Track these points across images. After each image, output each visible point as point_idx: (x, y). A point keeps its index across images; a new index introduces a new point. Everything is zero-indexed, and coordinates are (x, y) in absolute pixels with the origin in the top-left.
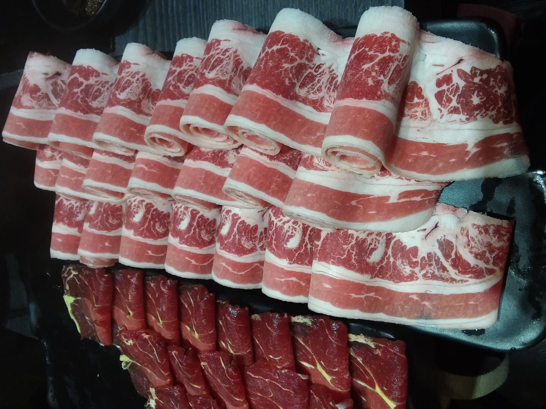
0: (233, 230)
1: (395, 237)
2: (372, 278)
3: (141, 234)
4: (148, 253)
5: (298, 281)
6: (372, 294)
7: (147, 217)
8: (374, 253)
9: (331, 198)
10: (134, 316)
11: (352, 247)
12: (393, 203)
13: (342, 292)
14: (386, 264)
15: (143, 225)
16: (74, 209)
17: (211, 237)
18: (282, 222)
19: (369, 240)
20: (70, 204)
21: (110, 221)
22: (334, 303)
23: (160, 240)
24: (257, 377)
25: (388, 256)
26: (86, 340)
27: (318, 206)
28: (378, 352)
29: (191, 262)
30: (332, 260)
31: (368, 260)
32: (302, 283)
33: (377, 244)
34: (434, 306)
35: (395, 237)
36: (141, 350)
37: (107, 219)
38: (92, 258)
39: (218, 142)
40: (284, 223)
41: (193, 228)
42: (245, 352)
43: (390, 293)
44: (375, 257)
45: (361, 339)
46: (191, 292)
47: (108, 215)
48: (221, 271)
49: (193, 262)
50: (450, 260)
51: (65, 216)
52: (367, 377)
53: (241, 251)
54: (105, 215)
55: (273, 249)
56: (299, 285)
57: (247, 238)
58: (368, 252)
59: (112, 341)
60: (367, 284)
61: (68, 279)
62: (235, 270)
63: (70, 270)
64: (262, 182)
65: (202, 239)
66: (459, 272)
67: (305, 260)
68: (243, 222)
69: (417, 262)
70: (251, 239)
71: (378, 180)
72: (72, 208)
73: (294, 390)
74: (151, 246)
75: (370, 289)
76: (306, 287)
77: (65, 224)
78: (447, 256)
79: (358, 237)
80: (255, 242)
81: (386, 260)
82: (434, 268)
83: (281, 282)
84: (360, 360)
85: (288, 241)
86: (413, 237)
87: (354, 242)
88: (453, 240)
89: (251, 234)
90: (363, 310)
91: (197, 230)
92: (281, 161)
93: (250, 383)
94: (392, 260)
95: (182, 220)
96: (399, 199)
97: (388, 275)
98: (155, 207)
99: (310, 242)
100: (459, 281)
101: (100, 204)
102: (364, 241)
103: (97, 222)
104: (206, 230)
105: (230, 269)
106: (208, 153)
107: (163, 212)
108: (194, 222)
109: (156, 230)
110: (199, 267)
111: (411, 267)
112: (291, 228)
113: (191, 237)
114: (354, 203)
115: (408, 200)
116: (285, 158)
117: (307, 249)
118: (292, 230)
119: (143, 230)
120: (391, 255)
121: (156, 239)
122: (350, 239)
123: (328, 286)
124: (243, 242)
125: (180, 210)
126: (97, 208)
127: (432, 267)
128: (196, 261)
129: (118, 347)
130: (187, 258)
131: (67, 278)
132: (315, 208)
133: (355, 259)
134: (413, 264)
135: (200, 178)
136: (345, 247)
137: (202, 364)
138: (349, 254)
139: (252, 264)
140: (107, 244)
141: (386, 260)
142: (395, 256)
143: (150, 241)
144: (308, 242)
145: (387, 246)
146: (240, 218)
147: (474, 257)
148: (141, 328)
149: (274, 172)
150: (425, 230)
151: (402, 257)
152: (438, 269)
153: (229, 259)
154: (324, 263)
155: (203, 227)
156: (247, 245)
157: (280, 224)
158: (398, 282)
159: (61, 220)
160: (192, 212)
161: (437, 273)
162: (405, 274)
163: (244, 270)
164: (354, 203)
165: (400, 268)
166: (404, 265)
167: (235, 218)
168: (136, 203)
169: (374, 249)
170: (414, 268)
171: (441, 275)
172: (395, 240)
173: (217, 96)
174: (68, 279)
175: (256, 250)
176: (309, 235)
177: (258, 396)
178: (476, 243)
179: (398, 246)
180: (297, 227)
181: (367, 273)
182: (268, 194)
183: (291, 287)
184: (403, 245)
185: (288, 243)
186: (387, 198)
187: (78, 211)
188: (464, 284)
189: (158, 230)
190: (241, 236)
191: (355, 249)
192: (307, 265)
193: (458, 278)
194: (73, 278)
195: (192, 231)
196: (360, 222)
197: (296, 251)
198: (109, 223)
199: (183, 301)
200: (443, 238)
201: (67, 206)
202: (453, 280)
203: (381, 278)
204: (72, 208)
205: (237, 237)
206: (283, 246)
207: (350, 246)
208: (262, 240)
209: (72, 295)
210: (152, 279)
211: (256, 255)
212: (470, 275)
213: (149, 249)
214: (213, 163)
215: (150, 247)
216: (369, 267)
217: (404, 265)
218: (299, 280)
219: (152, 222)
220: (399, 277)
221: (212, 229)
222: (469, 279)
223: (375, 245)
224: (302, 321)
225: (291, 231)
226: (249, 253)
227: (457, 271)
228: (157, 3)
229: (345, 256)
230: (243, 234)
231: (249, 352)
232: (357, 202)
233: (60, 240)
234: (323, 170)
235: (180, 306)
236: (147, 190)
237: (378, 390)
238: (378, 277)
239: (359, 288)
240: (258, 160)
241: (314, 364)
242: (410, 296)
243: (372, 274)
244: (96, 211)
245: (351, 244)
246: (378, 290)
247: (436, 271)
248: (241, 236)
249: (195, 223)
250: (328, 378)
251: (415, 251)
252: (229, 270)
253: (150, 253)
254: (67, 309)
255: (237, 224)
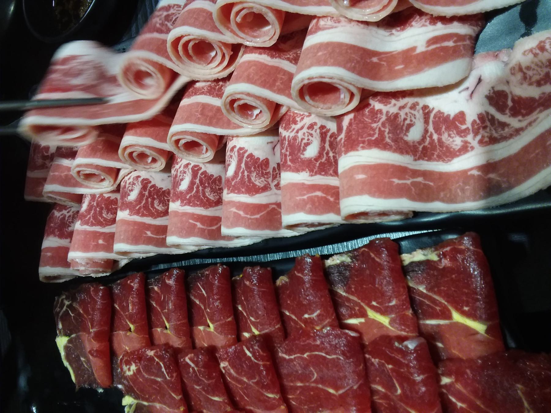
0: (241, 167)
1: (433, 109)
2: (415, 160)
3: (138, 213)
4: (146, 234)
5: (324, 195)
6: (420, 179)
7: (144, 194)
8: (412, 130)
9: (347, 52)
10: (136, 331)
11: (383, 124)
12: (422, 53)
13: (380, 180)
14: (430, 143)
15: (140, 203)
16: (66, 219)
17: (218, 197)
18: (295, 131)
19: (402, 114)
20: (61, 215)
21: (104, 215)
22: (372, 194)
23: (160, 219)
24: (292, 357)
25: (429, 134)
26: (82, 389)
27: (332, 61)
28: (446, 262)
29: (197, 225)
30: (361, 145)
31: (406, 138)
32: (329, 197)
33: (413, 119)
34: (501, 175)
35: (433, 109)
36: (146, 376)
37: (101, 213)
38: (82, 258)
39: (212, 69)
40: (297, 132)
41: (195, 186)
42: (273, 328)
43: (442, 175)
44: (414, 135)
45: (419, 256)
46: (202, 281)
47: (102, 209)
48: (231, 219)
49: (199, 225)
50: (507, 111)
51: (56, 228)
52: (438, 308)
53: (253, 190)
54: (98, 209)
55: (290, 166)
56: (327, 201)
57: (257, 174)
58: (404, 128)
59: (112, 381)
60: (411, 167)
61: (61, 314)
62: (247, 214)
63: (62, 300)
64: (265, 80)
65: (207, 197)
66: (524, 116)
67: (329, 170)
68: (251, 156)
69: (468, 129)
70: (263, 175)
71: (397, 36)
72: (64, 218)
73: (343, 353)
74: (150, 226)
75: (415, 173)
76: (335, 202)
77: (55, 236)
78: (501, 109)
79: (387, 112)
80: (268, 178)
81: (428, 139)
82: (490, 130)
83: (304, 200)
84: (422, 288)
85: (304, 150)
86: (456, 101)
87: (384, 118)
88: (505, 88)
89: (262, 169)
90: (413, 198)
91: (200, 188)
92: (283, 59)
93: (284, 371)
94: (435, 137)
95: (182, 180)
96: (428, 46)
97: (435, 156)
98: (153, 183)
99: (332, 149)
100: (526, 127)
101: (93, 196)
102: (396, 116)
103: (90, 218)
104: (212, 188)
105: (241, 213)
106: (203, 88)
107: (162, 188)
108: (195, 179)
109: (155, 208)
110: (206, 231)
111: (461, 136)
112: (306, 134)
113: (194, 196)
114: (375, 60)
115: (438, 45)
116: (288, 56)
117: (329, 157)
118: (308, 136)
119: (140, 208)
120: (433, 131)
121: (155, 218)
122: (379, 115)
123: (361, 176)
124: (253, 179)
125: (179, 171)
126: (90, 203)
127: (488, 129)
128: (202, 223)
129: (120, 386)
130: (191, 221)
131: (59, 312)
132: (329, 63)
133: (389, 137)
134: (462, 133)
135: (197, 111)
136: (374, 125)
137: (222, 365)
138: (381, 133)
139: (266, 206)
140: (101, 242)
141: (428, 139)
142: (437, 130)
143: (148, 220)
144: (329, 149)
145: (426, 122)
146: (247, 151)
147: (537, 86)
148: (144, 347)
149: (278, 70)
150: (468, 88)
151: (448, 128)
152: (495, 129)
153: (239, 202)
154: (352, 153)
155: (207, 185)
156: (259, 182)
157: (292, 135)
158: (450, 161)
159: (53, 233)
160: (192, 169)
161: (495, 135)
162: (454, 147)
163: (258, 213)
164: (375, 60)
165: (448, 142)
166: (453, 138)
167: (241, 152)
168: (131, 180)
169: (410, 126)
170: (465, 136)
171: (501, 135)
172: (434, 112)
173: (205, 8)
174: (61, 314)
175: (271, 189)
176: (330, 141)
177: (297, 388)
178: (534, 69)
179: (439, 118)
180: (313, 132)
181: (407, 153)
182: (274, 91)
183: (317, 204)
184: (445, 115)
185: (305, 153)
186: (414, 49)
187: (71, 220)
188: (534, 124)
189: (157, 207)
190: (250, 172)
191: (387, 125)
192: (332, 176)
193: (523, 124)
194: (66, 310)
195: (195, 190)
196: (386, 80)
197: (316, 159)
198: (102, 217)
199: (193, 298)
200: (492, 91)
201: (59, 217)
202: (518, 131)
203: (427, 160)
204: (64, 218)
205: (246, 173)
206: (299, 157)
207: (380, 124)
208: (276, 177)
209: (66, 335)
210: (155, 280)
211: (271, 195)
212: (538, 110)
213: (148, 230)
214: (210, 95)
215: (149, 227)
216: (409, 146)
217: (453, 138)
218: (326, 194)
219: (150, 200)
220: (449, 154)
221: (217, 187)
222: (537, 116)
223: (411, 121)
224: (338, 262)
225: (306, 138)
226: (262, 192)
227: (520, 118)
228: (147, 3)
229: (376, 136)
230: (253, 169)
231: (278, 328)
232: (378, 59)
233: (49, 254)
234: (332, 28)
235: (190, 305)
236: (140, 146)
237: (457, 317)
238: (423, 159)
239: (401, 171)
240: (257, 59)
241: (363, 314)
242: (469, 173)
243: (415, 155)
244: (88, 206)
245: (382, 120)
246: (425, 174)
247: (494, 132)
248: (250, 172)
249: (197, 181)
250: (384, 320)
251: (461, 116)
252: (240, 215)
253: (149, 233)
254: (59, 354)
255: (245, 158)
